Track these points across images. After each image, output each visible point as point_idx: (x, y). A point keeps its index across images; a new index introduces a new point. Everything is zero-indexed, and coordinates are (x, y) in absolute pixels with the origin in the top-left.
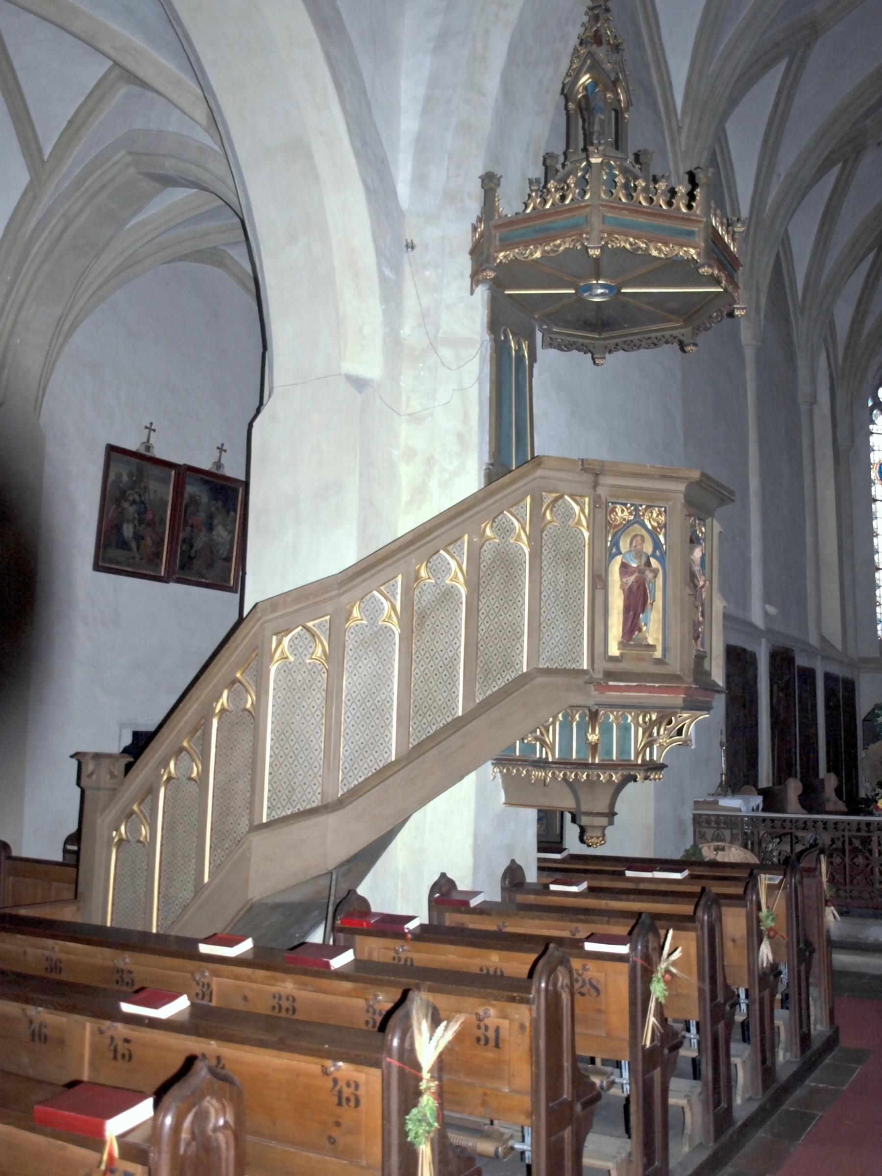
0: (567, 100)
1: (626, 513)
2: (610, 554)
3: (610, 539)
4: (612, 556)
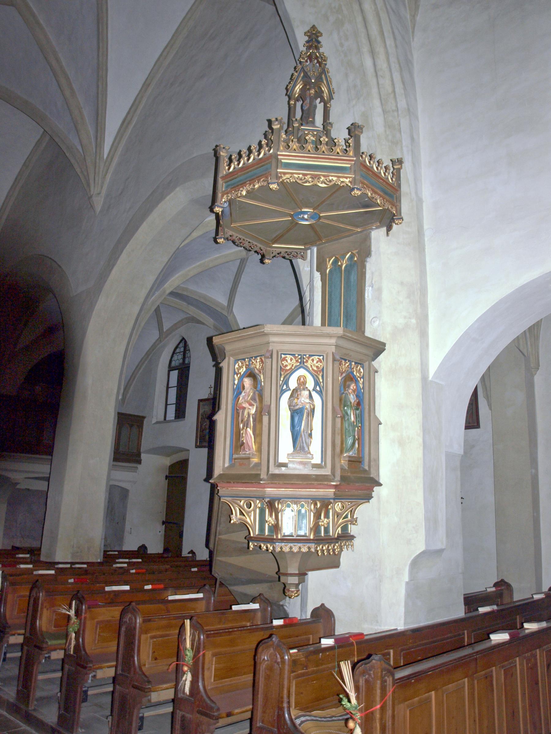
0: (290, 98)
1: (294, 361)
2: (282, 390)
3: (282, 379)
4: (283, 392)
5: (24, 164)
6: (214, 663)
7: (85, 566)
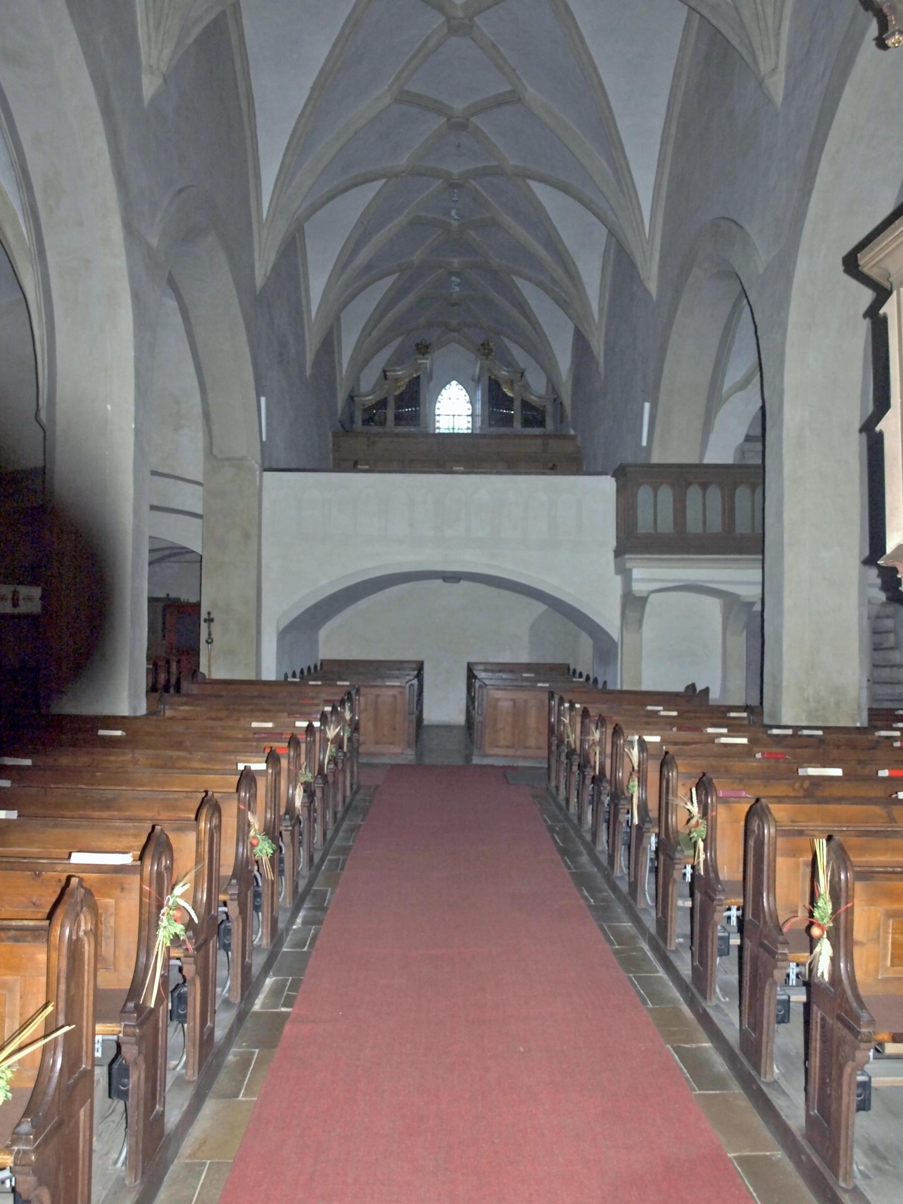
5: (675, 76)
6: (890, 931)
7: (820, 733)
